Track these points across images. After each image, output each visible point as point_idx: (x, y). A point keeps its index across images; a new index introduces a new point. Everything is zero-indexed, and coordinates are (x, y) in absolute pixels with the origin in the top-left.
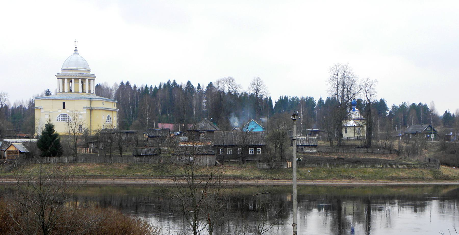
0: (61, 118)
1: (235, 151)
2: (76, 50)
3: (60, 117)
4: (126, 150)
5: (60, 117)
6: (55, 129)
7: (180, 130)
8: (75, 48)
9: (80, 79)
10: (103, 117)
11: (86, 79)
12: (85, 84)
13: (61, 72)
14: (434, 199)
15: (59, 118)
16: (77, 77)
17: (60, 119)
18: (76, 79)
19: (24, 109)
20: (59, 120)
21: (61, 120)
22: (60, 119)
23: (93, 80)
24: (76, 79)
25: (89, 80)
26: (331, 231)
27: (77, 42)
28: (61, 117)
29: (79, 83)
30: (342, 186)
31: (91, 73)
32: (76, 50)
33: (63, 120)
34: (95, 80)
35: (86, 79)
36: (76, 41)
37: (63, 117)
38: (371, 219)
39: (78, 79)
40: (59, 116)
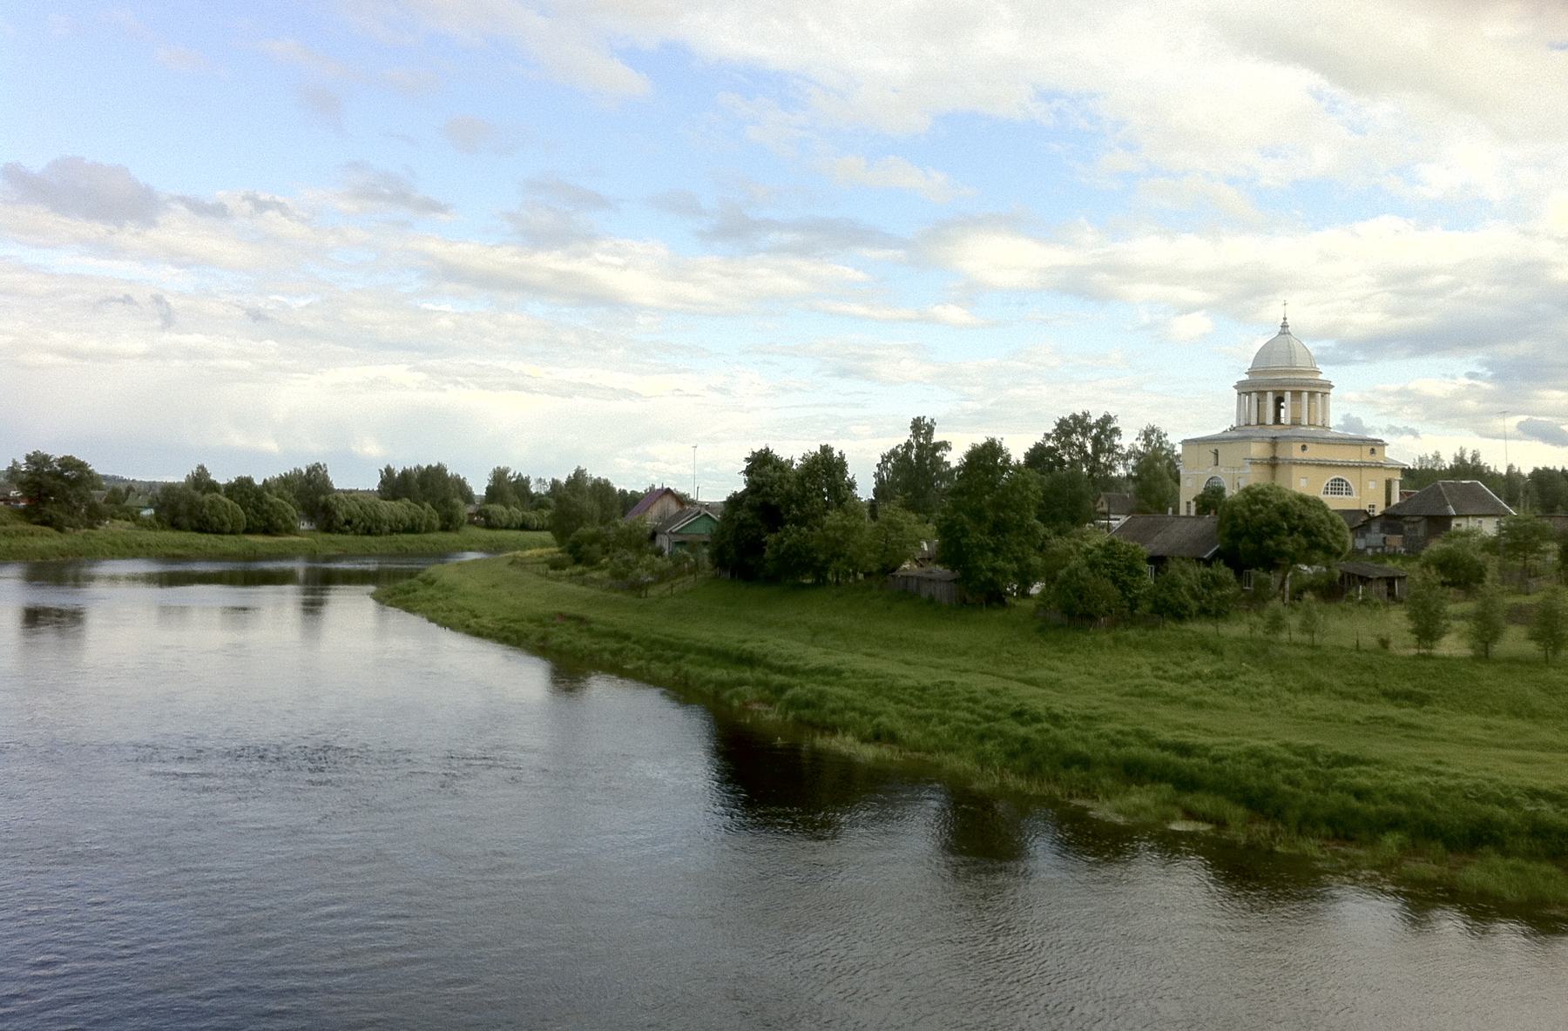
0: (1332, 489)
1: (1375, 552)
3: (1330, 486)
4: (75, 508)
5: (1330, 486)
7: (1503, 507)
9: (1286, 393)
10: (1372, 485)
11: (1318, 392)
13: (1246, 377)
14: (350, 578)
15: (1327, 489)
16: (1298, 389)
17: (1329, 491)
19: (1557, 471)
20: (1327, 493)
21: (1346, 494)
22: (1329, 491)
23: (1324, 394)
25: (1312, 394)
26: (555, 682)
28: (1332, 484)
30: (281, 560)
31: (1321, 377)
33: (1335, 493)
34: (1329, 394)
35: (1318, 392)
38: (478, 639)
39: (1300, 392)
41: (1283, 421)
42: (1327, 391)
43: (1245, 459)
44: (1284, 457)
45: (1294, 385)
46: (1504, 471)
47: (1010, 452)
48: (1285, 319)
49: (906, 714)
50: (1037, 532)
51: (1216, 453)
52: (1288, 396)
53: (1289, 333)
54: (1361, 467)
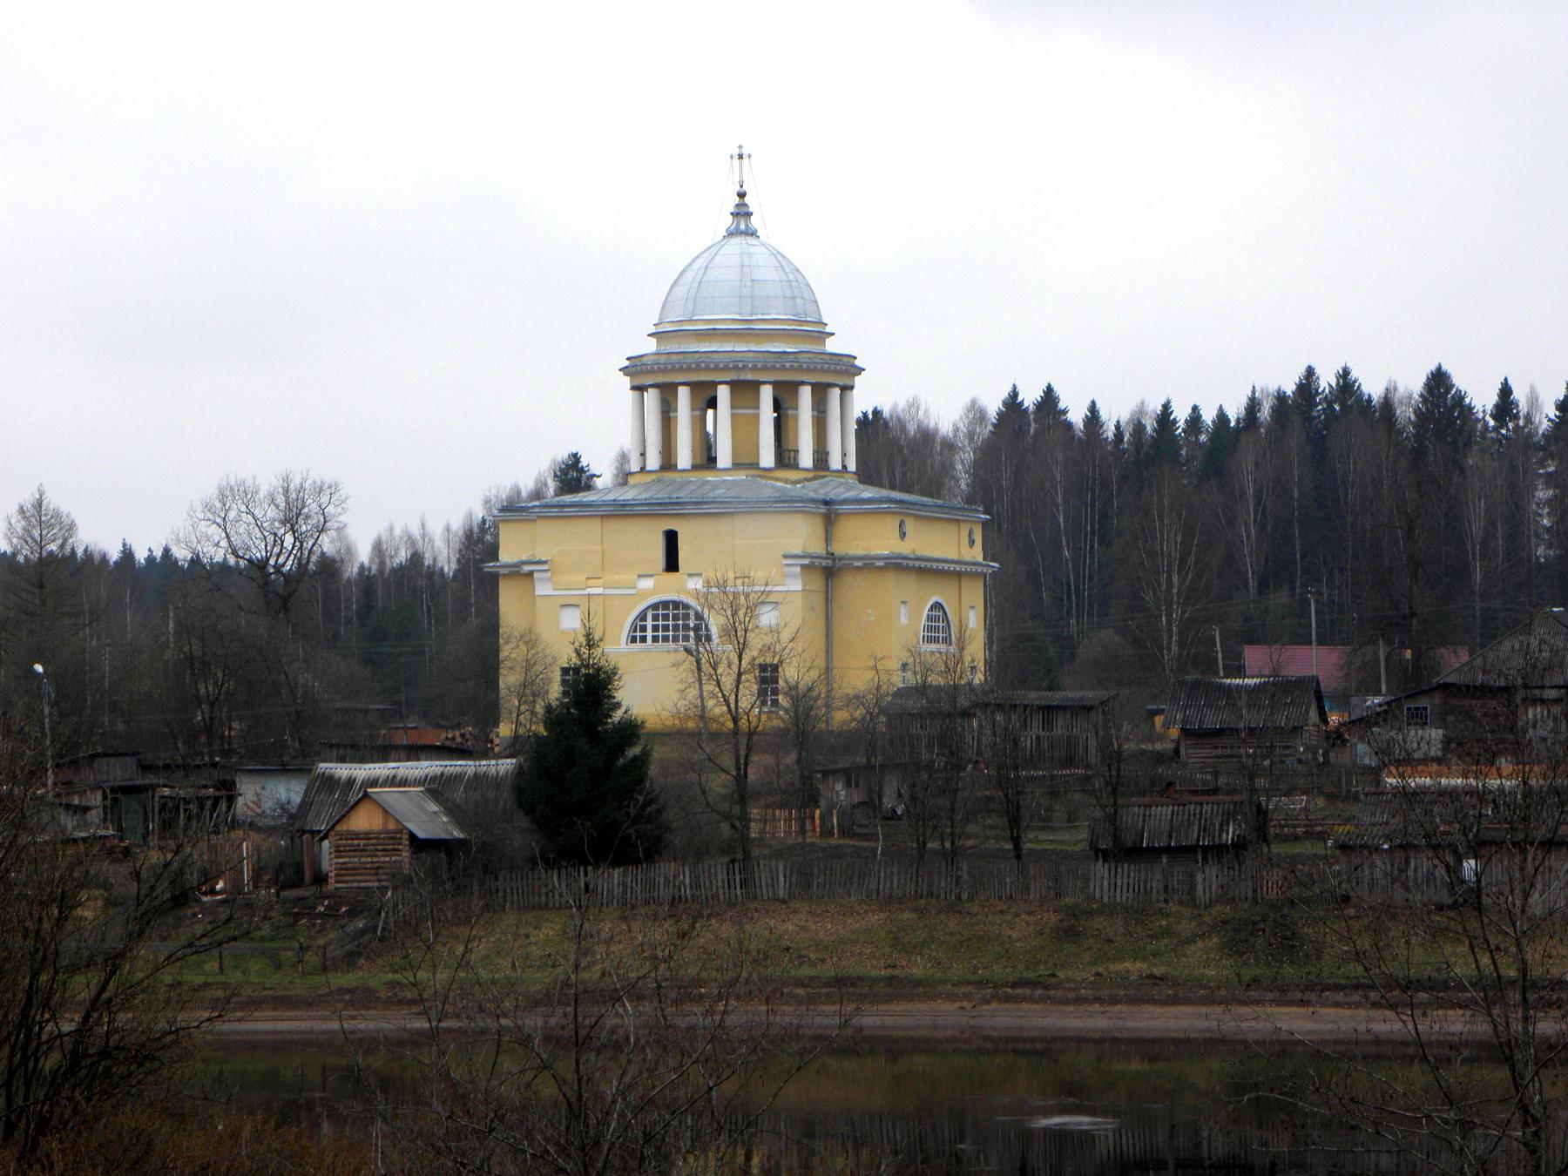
0: (655, 628)
2: (742, 212)
3: (649, 623)
5: (649, 623)
6: (619, 695)
8: (737, 200)
11: (803, 383)
12: (676, 418)
13: (650, 346)
15: (644, 629)
16: (749, 377)
17: (649, 634)
18: (745, 391)
20: (644, 639)
21: (655, 639)
22: (649, 634)
24: (745, 391)
27: (746, 160)
28: (655, 618)
29: (758, 407)
32: (742, 212)
34: (852, 388)
36: (741, 157)
37: (666, 617)
39: (755, 386)
40: (643, 617)
41: (835, 462)
42: (846, 382)
43: (785, 557)
44: (843, 553)
45: (698, 369)
46: (114, 555)
47: (73, 516)
48: (742, 195)
49: (280, 1121)
50: (1429, 788)
51: (671, 539)
52: (723, 393)
53: (753, 234)
54: (959, 575)
